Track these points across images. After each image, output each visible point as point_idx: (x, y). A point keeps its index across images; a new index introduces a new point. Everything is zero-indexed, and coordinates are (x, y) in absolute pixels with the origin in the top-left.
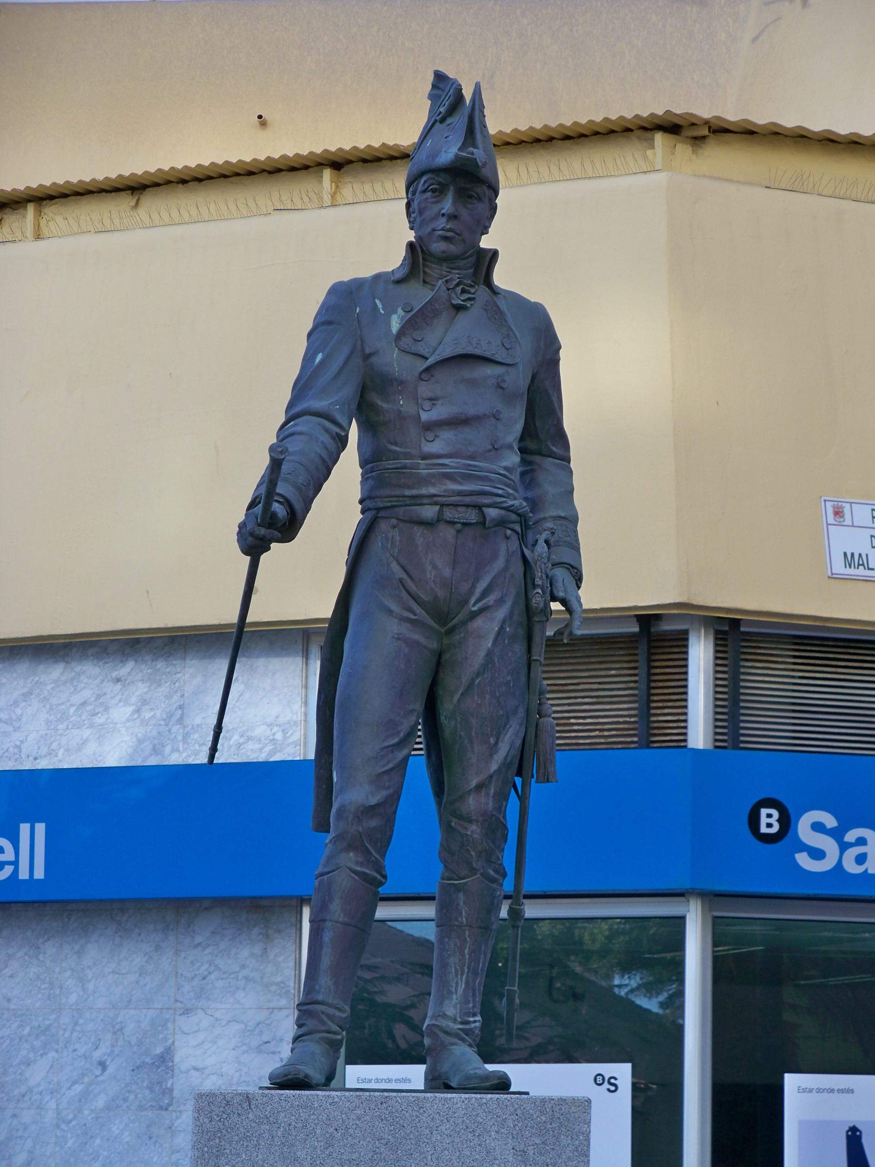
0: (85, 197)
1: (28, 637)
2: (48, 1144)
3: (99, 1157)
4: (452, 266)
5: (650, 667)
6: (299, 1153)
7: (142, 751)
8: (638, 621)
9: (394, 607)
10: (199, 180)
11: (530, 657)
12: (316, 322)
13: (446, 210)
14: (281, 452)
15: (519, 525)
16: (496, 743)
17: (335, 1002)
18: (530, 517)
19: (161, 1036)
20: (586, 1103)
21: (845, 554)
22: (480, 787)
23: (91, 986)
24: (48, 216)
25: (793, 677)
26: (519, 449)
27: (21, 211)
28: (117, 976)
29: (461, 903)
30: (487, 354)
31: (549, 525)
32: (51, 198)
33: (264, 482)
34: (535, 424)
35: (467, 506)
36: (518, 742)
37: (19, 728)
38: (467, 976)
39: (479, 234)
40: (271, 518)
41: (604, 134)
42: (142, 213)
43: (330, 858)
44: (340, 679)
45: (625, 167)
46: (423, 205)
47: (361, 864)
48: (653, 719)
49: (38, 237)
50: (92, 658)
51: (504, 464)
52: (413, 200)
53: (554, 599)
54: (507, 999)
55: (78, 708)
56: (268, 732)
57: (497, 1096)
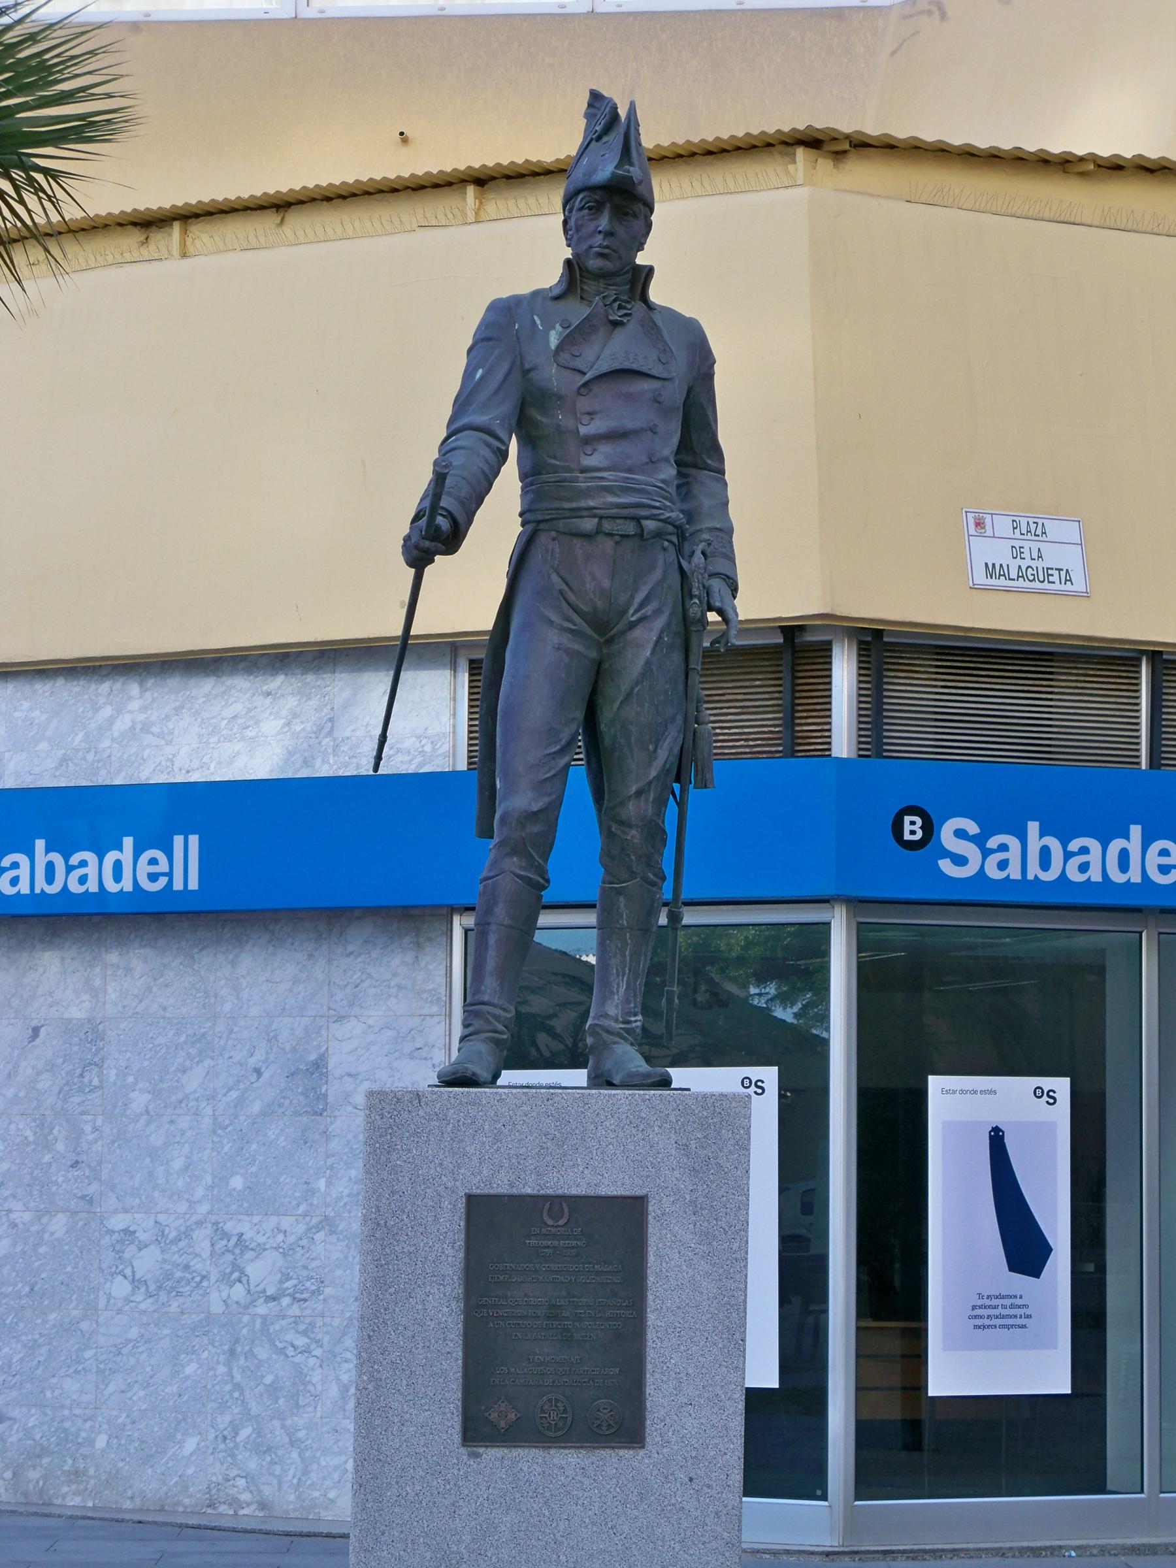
0: (229, 215)
1: (179, 652)
2: (205, 1149)
3: (255, 1161)
4: (609, 282)
5: (794, 678)
6: (468, 1148)
7: (293, 763)
8: (782, 632)
9: (554, 617)
10: (344, 197)
11: (687, 666)
12: (477, 337)
13: (603, 226)
14: (445, 466)
15: (675, 536)
16: (655, 750)
17: (501, 1003)
18: (687, 529)
19: (315, 1043)
20: (747, 1099)
21: (986, 564)
22: (639, 793)
23: (245, 995)
24: (194, 234)
25: (936, 686)
26: (675, 462)
27: (167, 229)
28: (270, 984)
29: (622, 906)
30: (645, 369)
31: (705, 536)
32: (197, 216)
33: (428, 495)
34: (690, 438)
35: (625, 518)
36: (676, 750)
37: (171, 742)
38: (628, 978)
39: (635, 250)
40: (435, 531)
41: (745, 149)
42: (287, 229)
43: (494, 863)
44: (502, 688)
45: (767, 181)
46: (580, 223)
47: (524, 869)
48: (797, 728)
49: (184, 255)
50: (242, 672)
51: (662, 476)
52: (570, 217)
53: (710, 609)
54: (667, 999)
55: (228, 722)
56: (418, 745)
57: (660, 1092)
